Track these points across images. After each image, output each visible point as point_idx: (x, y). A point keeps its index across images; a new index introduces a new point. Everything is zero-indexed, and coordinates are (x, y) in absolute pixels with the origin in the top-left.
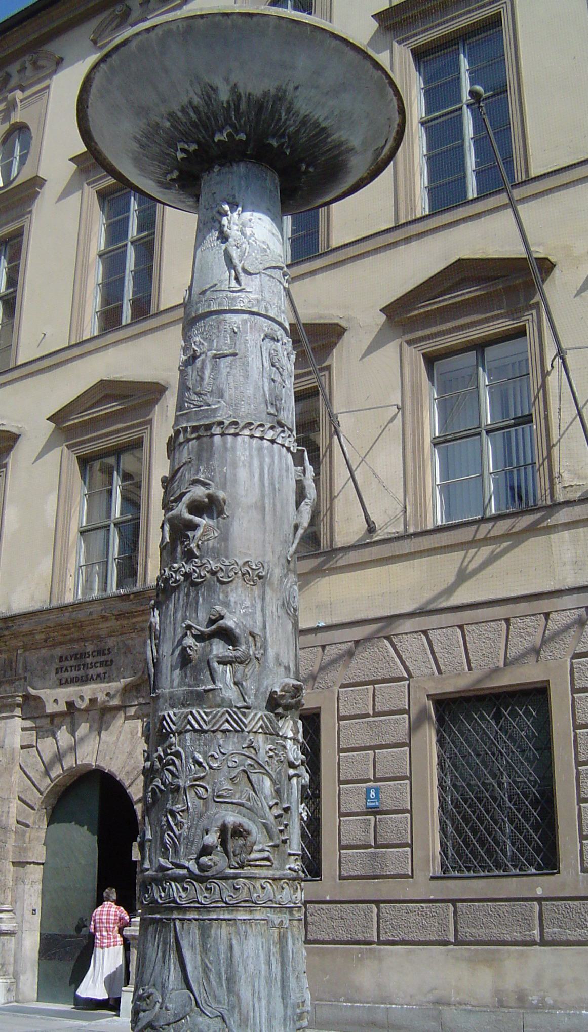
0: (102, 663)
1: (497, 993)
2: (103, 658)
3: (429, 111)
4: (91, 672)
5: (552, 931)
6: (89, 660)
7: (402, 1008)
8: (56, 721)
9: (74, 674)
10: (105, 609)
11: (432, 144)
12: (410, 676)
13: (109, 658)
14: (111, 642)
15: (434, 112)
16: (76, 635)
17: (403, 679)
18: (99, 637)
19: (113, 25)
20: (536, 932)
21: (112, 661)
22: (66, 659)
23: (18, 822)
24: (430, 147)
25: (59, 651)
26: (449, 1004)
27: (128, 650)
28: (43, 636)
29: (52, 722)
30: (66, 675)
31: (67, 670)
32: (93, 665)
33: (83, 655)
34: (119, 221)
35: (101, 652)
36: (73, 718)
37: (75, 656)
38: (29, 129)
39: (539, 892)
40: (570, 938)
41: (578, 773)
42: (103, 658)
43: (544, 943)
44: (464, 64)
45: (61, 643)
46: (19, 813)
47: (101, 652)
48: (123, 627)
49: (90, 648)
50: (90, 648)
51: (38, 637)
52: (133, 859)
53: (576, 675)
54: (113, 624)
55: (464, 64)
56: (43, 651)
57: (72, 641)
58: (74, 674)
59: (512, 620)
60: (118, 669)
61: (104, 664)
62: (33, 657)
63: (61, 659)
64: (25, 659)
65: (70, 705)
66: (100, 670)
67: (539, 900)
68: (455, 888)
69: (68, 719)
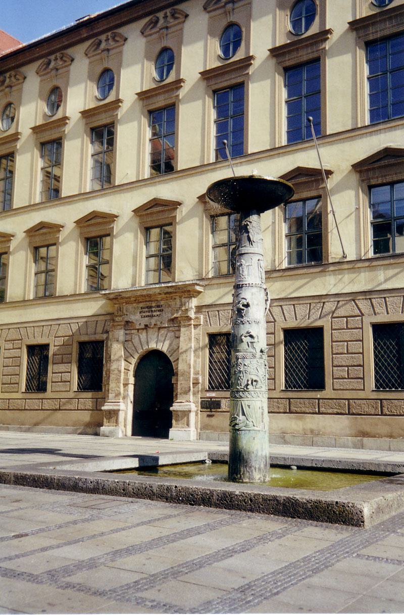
0: (159, 311)
1: (304, 429)
2: (159, 309)
3: (370, 74)
4: (154, 314)
5: (322, 410)
6: (153, 309)
7: (211, 410)
8: (140, 331)
9: (147, 314)
10: (161, 291)
11: (289, 112)
12: (275, 321)
13: (161, 308)
14: (162, 303)
15: (291, 97)
16: (148, 300)
17: (272, 322)
18: (157, 300)
19: (151, 27)
20: (317, 410)
21: (163, 310)
22: (144, 308)
23: (125, 369)
24: (371, 90)
25: (141, 305)
26: (287, 433)
27: (169, 306)
28: (134, 299)
29: (138, 331)
30: (144, 314)
31: (144, 312)
32: (155, 311)
33: (151, 307)
34: (110, 138)
35: (158, 306)
36: (147, 330)
37: (147, 307)
38: (111, 70)
39: (319, 396)
40: (329, 412)
41: (332, 358)
42: (159, 309)
43: (319, 413)
44: (305, 76)
45: (141, 302)
46: (125, 366)
47: (158, 306)
48: (167, 297)
49: (154, 305)
50: (154, 305)
51: (132, 299)
52: (173, 382)
53: (333, 324)
54: (163, 296)
55: (305, 76)
56: (134, 304)
57: (146, 301)
58: (147, 314)
59: (312, 304)
60: (165, 313)
61: (159, 311)
62: (130, 307)
63: (142, 308)
64: (126, 308)
65: (146, 326)
66: (158, 313)
67: (319, 399)
68: (290, 395)
69: (145, 331)
